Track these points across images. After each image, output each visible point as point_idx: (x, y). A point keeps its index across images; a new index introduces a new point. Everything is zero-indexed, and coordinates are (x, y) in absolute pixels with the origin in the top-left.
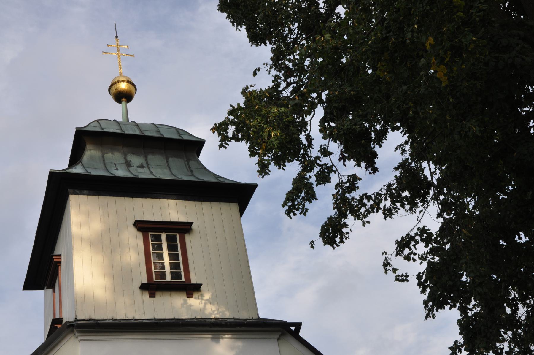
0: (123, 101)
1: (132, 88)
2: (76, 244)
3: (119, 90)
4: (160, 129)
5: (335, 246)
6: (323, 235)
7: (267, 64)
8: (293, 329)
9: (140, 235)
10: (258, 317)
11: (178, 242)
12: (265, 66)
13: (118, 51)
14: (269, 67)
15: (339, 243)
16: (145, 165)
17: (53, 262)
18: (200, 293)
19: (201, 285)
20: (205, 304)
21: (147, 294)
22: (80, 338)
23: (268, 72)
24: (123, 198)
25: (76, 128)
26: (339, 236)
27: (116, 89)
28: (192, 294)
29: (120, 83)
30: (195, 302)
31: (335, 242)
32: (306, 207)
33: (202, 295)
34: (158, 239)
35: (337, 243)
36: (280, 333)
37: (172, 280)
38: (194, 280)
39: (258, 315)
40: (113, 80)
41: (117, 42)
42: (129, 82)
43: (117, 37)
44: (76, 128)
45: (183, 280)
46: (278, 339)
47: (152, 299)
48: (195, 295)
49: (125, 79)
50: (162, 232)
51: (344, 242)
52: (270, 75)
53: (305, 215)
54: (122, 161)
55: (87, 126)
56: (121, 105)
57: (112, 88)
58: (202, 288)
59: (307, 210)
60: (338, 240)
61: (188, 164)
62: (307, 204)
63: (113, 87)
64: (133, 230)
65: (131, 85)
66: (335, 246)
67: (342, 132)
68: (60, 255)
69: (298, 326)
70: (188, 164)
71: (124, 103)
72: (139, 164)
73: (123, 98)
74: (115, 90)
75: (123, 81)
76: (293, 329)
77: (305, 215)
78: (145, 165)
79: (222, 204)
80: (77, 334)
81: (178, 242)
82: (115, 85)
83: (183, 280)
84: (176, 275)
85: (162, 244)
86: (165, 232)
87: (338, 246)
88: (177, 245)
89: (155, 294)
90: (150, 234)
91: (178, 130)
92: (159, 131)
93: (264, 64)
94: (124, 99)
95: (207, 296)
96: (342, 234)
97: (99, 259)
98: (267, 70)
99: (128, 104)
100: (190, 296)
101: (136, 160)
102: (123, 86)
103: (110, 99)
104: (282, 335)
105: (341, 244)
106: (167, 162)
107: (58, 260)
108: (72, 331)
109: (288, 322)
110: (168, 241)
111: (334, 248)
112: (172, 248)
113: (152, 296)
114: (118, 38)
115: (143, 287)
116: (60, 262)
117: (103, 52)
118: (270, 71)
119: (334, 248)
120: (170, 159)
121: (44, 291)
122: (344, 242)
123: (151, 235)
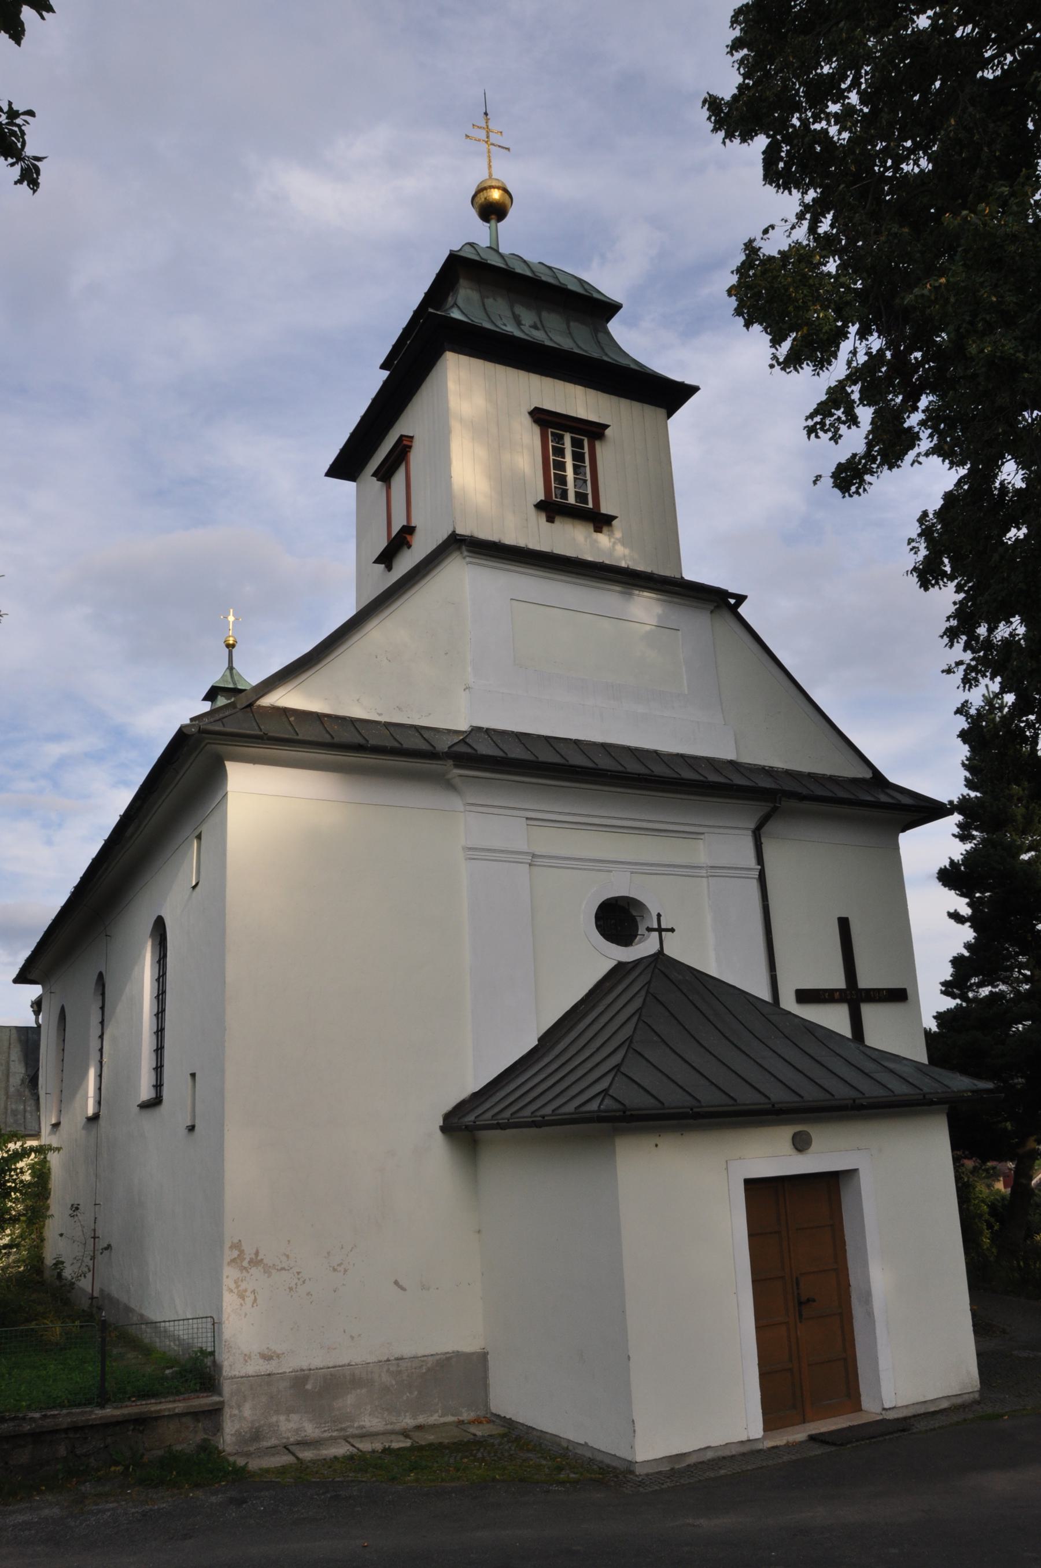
0: (492, 219)
1: (507, 200)
2: (456, 426)
3: (491, 200)
4: (558, 275)
5: (847, 494)
6: (835, 475)
7: (786, 221)
8: (732, 601)
9: (537, 430)
10: (682, 578)
11: (586, 450)
12: (783, 223)
13: (488, 137)
14: (790, 226)
15: (853, 493)
16: (539, 326)
17: (400, 447)
18: (610, 528)
19: (614, 518)
20: (614, 543)
21: (543, 518)
22: (468, 559)
23: (787, 233)
24: (516, 371)
25: (451, 251)
26: (857, 485)
27: (485, 199)
28: (602, 528)
29: (492, 190)
30: (603, 539)
31: (848, 490)
32: (840, 432)
33: (612, 531)
34: (560, 438)
35: (851, 492)
36: (715, 604)
37: (576, 502)
38: (605, 509)
39: (681, 574)
40: (481, 183)
41: (487, 123)
42: (505, 191)
43: (486, 114)
44: (451, 251)
45: (590, 505)
46: (712, 612)
47: (549, 524)
48: (605, 529)
49: (500, 185)
50: (566, 432)
51: (859, 494)
52: (789, 239)
53: (837, 443)
54: (508, 314)
55: (460, 250)
56: (488, 225)
57: (478, 195)
58: (614, 522)
59: (841, 436)
60: (853, 489)
61: (596, 336)
62: (843, 429)
63: (481, 194)
64: (527, 421)
65: (507, 197)
66: (847, 494)
67: (998, 354)
68: (412, 437)
69: (741, 599)
70: (596, 336)
71: (493, 222)
72: (531, 323)
73: (492, 213)
74: (483, 199)
75: (494, 187)
76: (732, 601)
77: (837, 443)
78: (539, 326)
79: (646, 406)
80: (466, 553)
81: (586, 450)
82: (485, 191)
83: (590, 505)
84: (581, 497)
85: (564, 448)
86: (570, 433)
87: (851, 496)
88: (584, 453)
89: (554, 518)
90: (550, 430)
91: (581, 282)
92: (557, 277)
93: (783, 220)
94: (493, 216)
95: (618, 534)
96: (862, 482)
97: (482, 452)
98: (786, 231)
99: (499, 224)
100: (598, 530)
101: (528, 317)
102: (496, 195)
103: (473, 214)
104: (718, 607)
105: (856, 496)
106: (569, 327)
107: (408, 443)
108: (459, 549)
109: (730, 591)
110: (573, 446)
111: (844, 497)
112: (578, 457)
113: (550, 520)
114: (488, 117)
115: (540, 506)
116: (410, 447)
117: (466, 135)
118: (790, 233)
119: (844, 497)
120: (572, 324)
121: (353, 484)
122: (859, 494)
123: (551, 432)
